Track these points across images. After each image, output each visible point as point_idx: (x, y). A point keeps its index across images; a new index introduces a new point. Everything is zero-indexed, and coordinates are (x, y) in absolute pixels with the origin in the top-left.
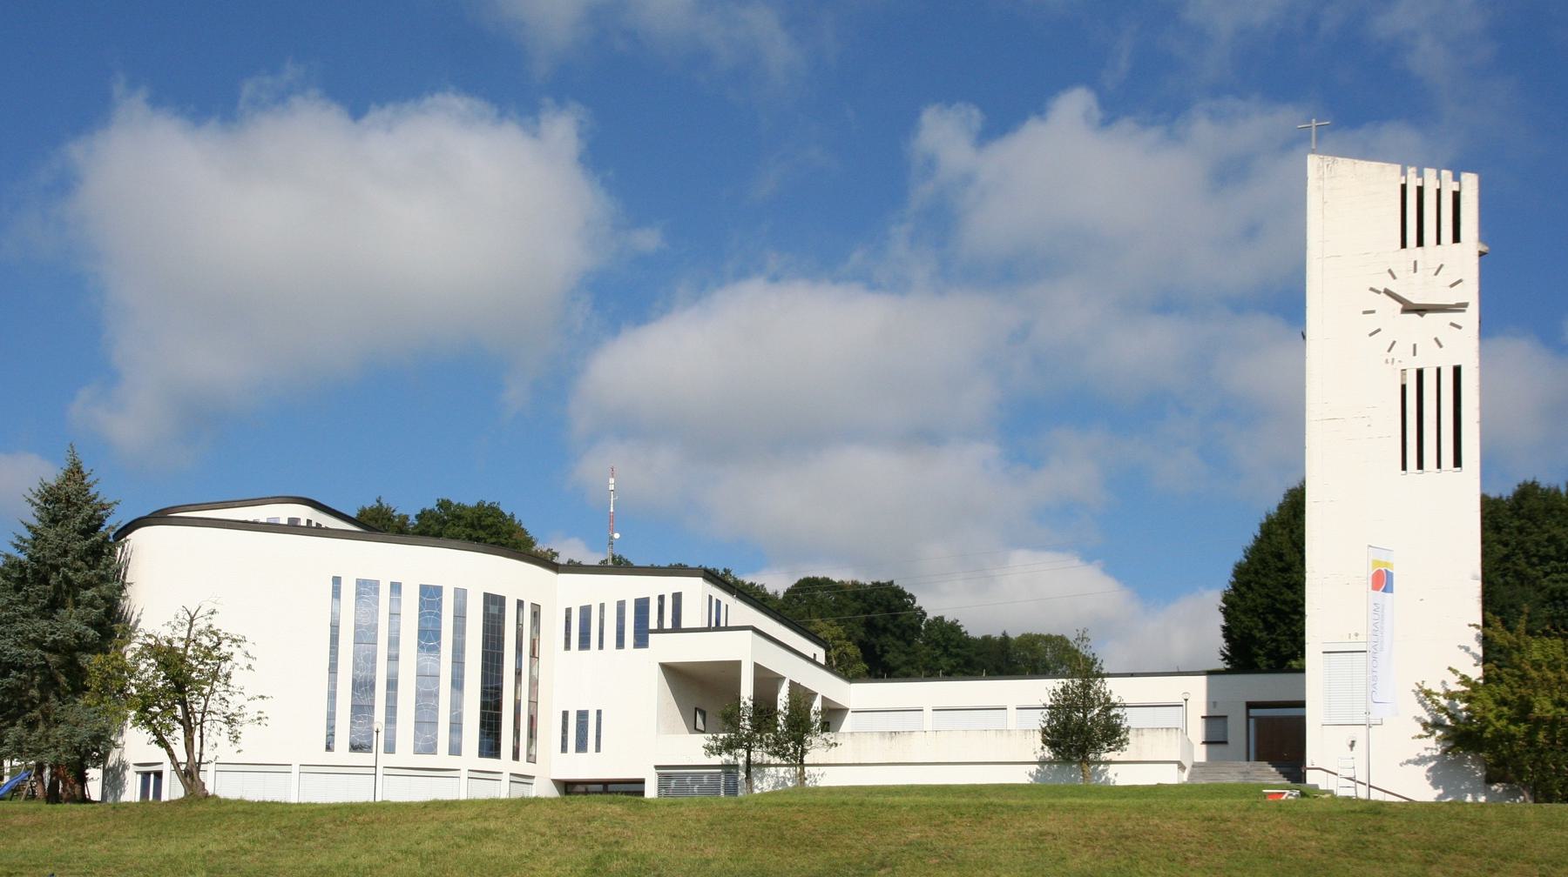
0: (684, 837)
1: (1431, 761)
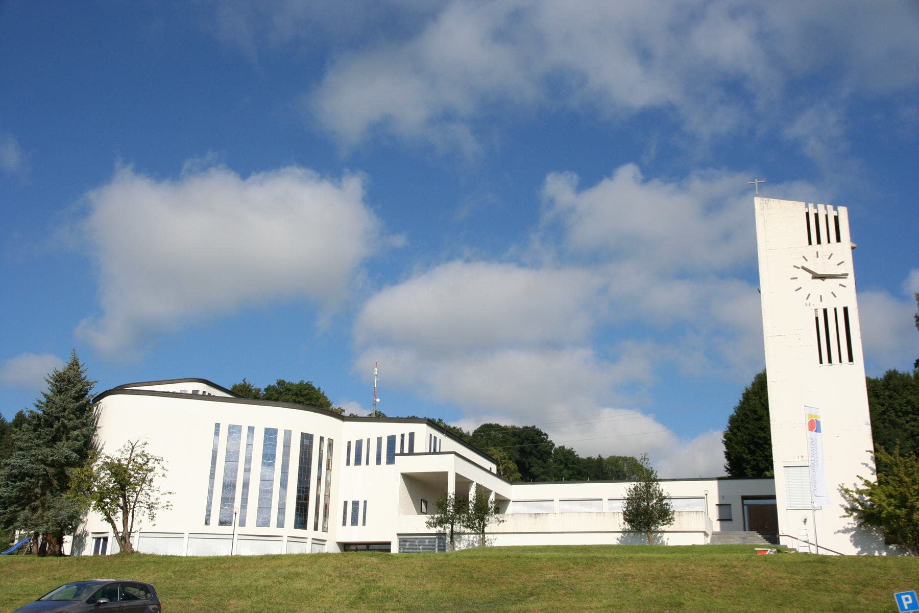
0: (414, 577)
1: (852, 531)
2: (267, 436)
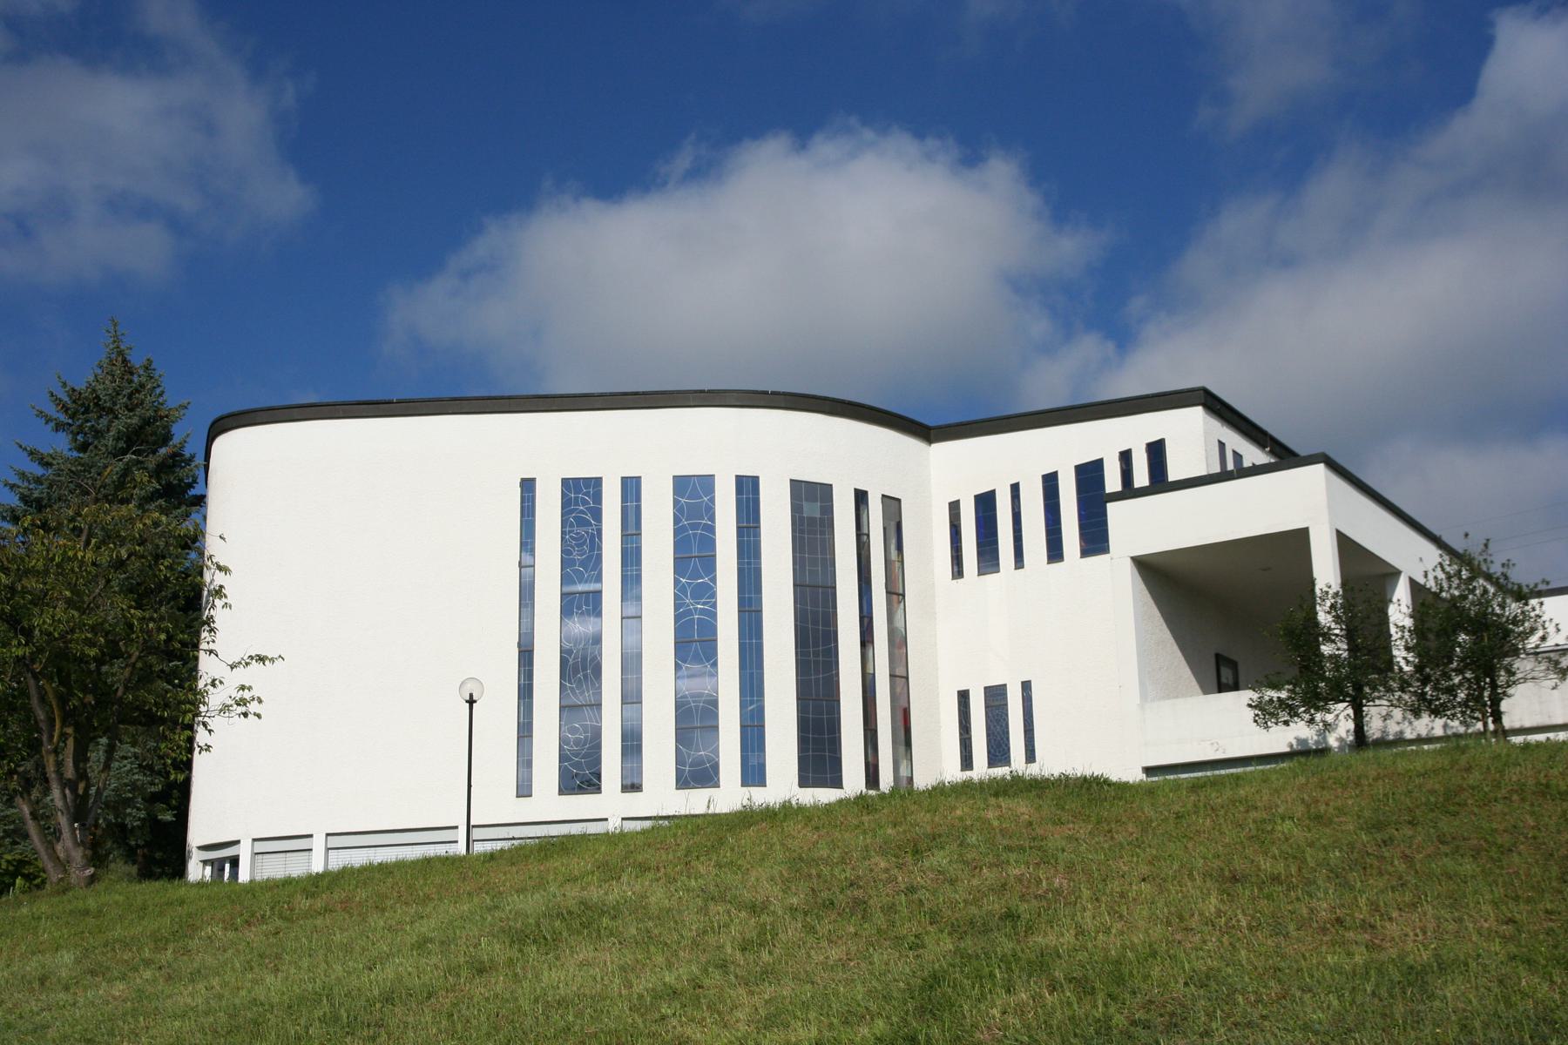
0: (1276, 879)
2: (683, 500)
